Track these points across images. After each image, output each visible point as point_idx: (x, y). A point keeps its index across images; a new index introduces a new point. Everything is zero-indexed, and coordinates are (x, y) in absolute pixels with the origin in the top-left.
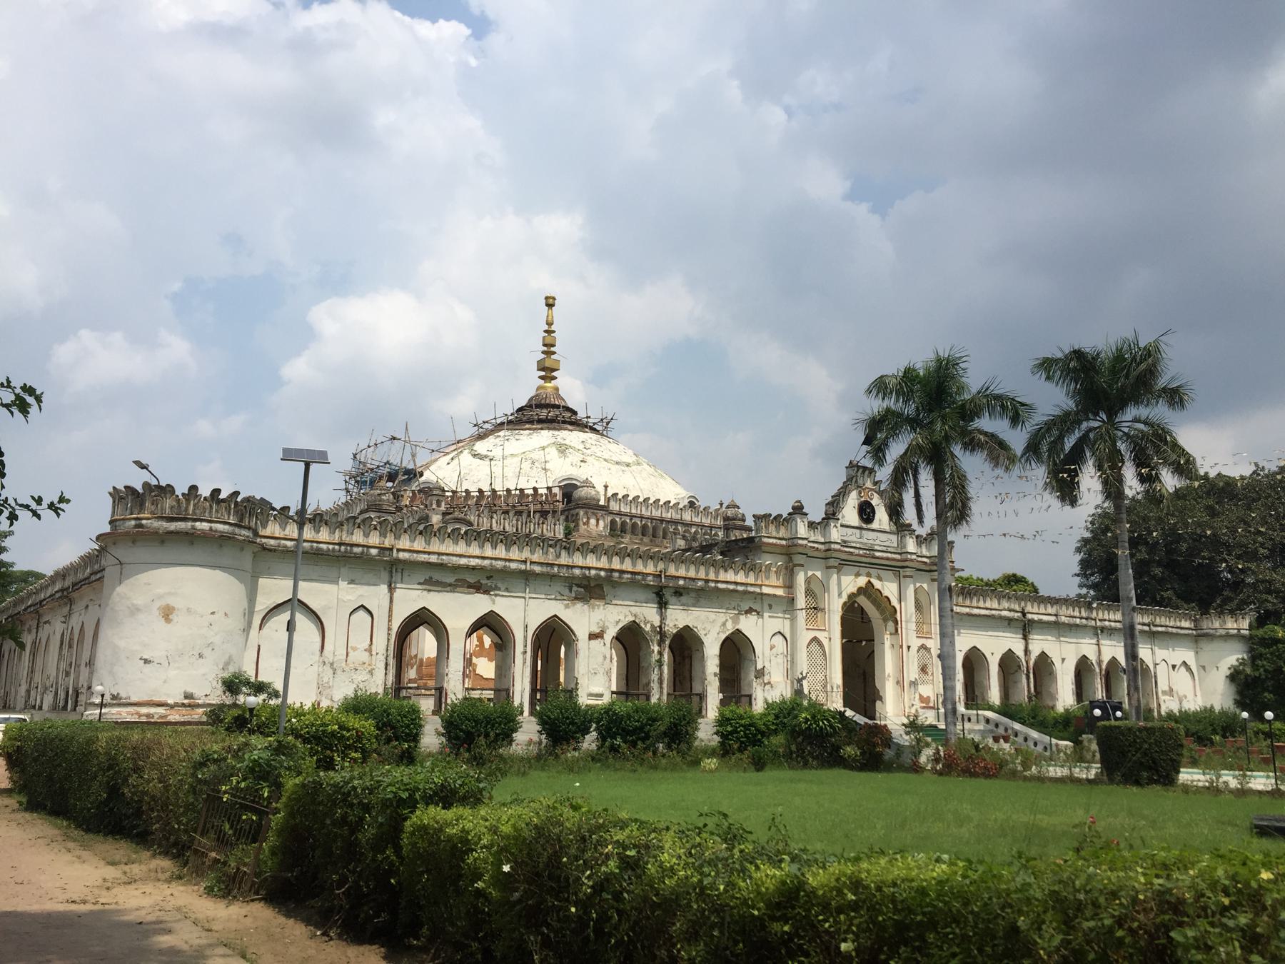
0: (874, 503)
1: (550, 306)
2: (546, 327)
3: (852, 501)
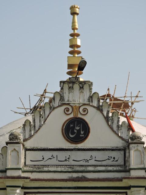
0: (87, 118)
1: (74, 13)
2: (72, 32)
3: (58, 118)
